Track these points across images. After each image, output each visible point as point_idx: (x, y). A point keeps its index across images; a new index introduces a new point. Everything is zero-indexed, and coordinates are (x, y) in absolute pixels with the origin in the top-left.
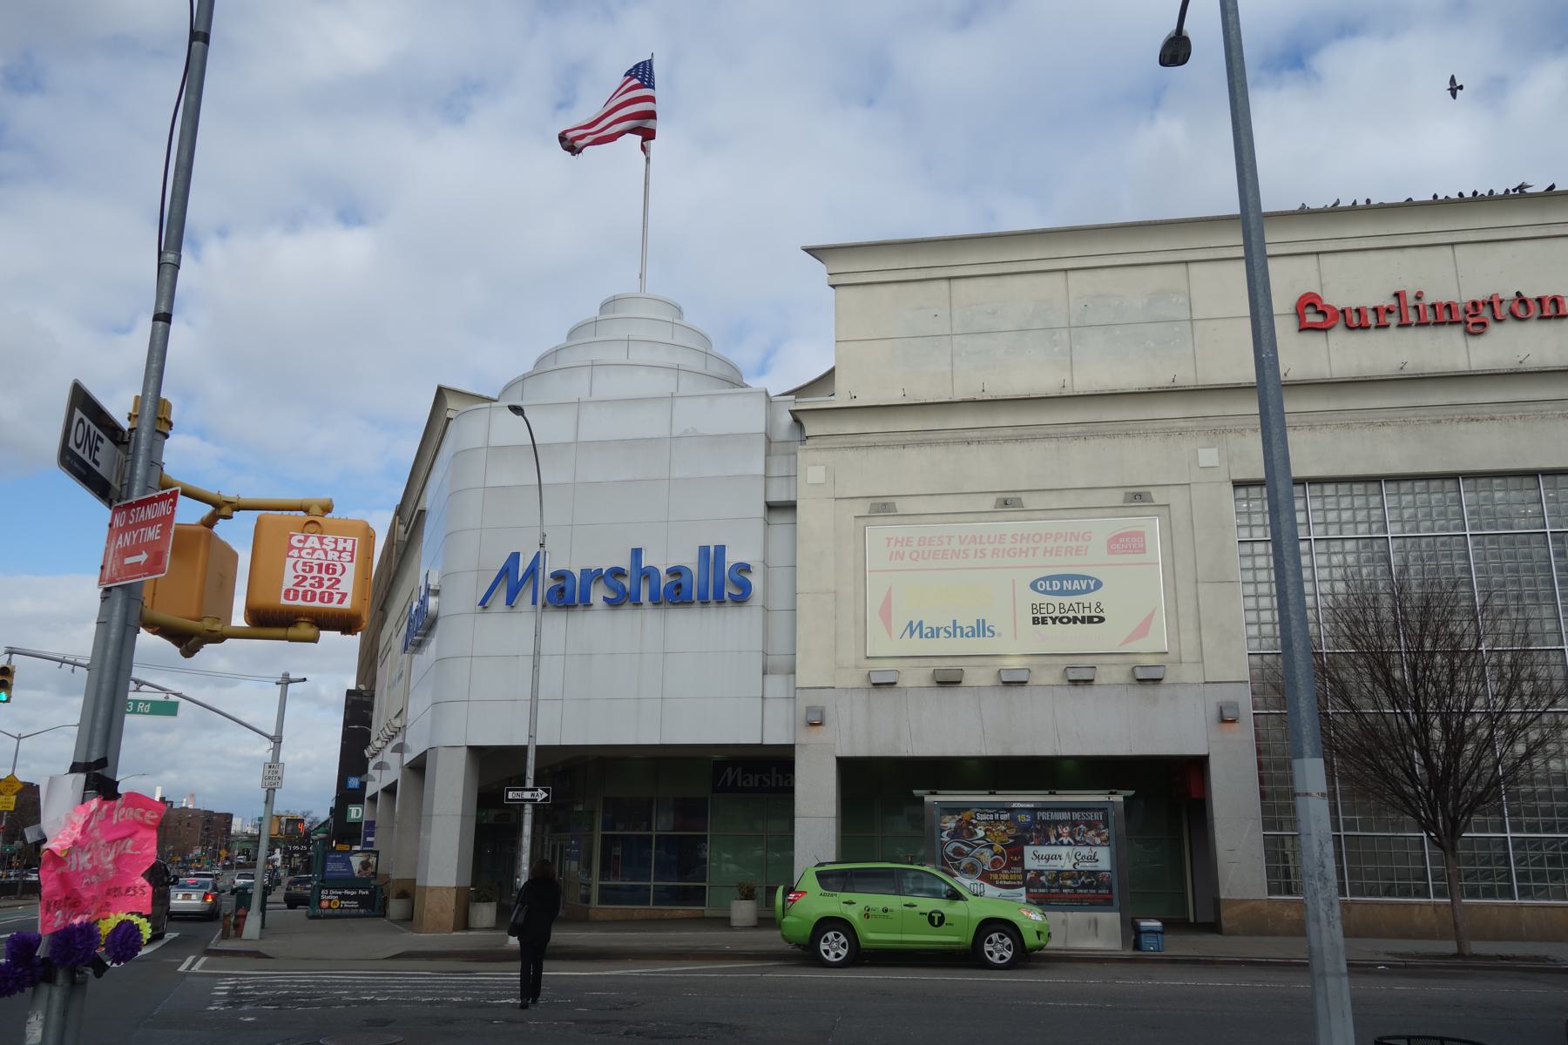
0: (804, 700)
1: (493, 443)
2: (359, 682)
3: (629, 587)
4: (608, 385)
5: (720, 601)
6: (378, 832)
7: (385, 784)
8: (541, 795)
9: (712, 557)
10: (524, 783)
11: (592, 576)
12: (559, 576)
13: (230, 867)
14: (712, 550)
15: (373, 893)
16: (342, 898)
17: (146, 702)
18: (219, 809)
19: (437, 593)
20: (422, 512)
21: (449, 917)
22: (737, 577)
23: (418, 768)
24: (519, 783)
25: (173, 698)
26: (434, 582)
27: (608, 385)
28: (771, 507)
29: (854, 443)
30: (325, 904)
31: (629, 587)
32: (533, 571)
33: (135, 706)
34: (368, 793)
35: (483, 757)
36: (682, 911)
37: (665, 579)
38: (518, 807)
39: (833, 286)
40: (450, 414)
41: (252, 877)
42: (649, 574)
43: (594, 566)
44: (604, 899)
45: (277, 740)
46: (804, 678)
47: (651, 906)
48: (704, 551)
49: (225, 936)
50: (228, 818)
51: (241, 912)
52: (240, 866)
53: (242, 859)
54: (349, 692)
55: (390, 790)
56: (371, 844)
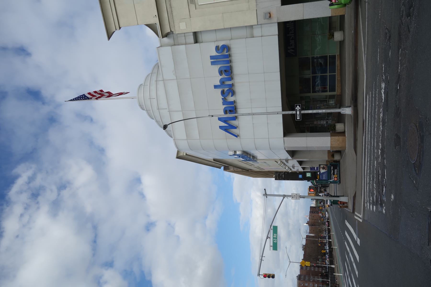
0: (262, 21)
1: (186, 138)
2: (272, 177)
3: (227, 89)
4: (163, 104)
5: (229, 56)
6: (313, 166)
7: (299, 165)
8: (298, 108)
9: (214, 60)
10: (294, 115)
11: (225, 101)
12: (226, 112)
13: (324, 206)
14: (212, 60)
15: (332, 165)
16: (334, 174)
17: (273, 235)
19: (235, 152)
20: (214, 160)
21: (340, 138)
22: (220, 51)
23: (293, 153)
24: (294, 116)
25: (272, 228)
26: (232, 153)
27: (163, 104)
28: (196, 41)
29: (170, 13)
31: (227, 89)
32: (225, 120)
33: (275, 238)
34: (302, 170)
35: (287, 132)
36: (338, 63)
37: (224, 76)
38: (303, 115)
39: (120, 28)
40: (185, 154)
41: (327, 201)
42: (222, 82)
43: (221, 101)
44: (334, 91)
45: (284, 196)
46: (254, 22)
47: (336, 74)
48: (213, 63)
49: (347, 207)
50: (311, 207)
51: (339, 203)
52: (324, 204)
53: (322, 203)
54: (276, 179)
55: (301, 163)
56: (317, 168)
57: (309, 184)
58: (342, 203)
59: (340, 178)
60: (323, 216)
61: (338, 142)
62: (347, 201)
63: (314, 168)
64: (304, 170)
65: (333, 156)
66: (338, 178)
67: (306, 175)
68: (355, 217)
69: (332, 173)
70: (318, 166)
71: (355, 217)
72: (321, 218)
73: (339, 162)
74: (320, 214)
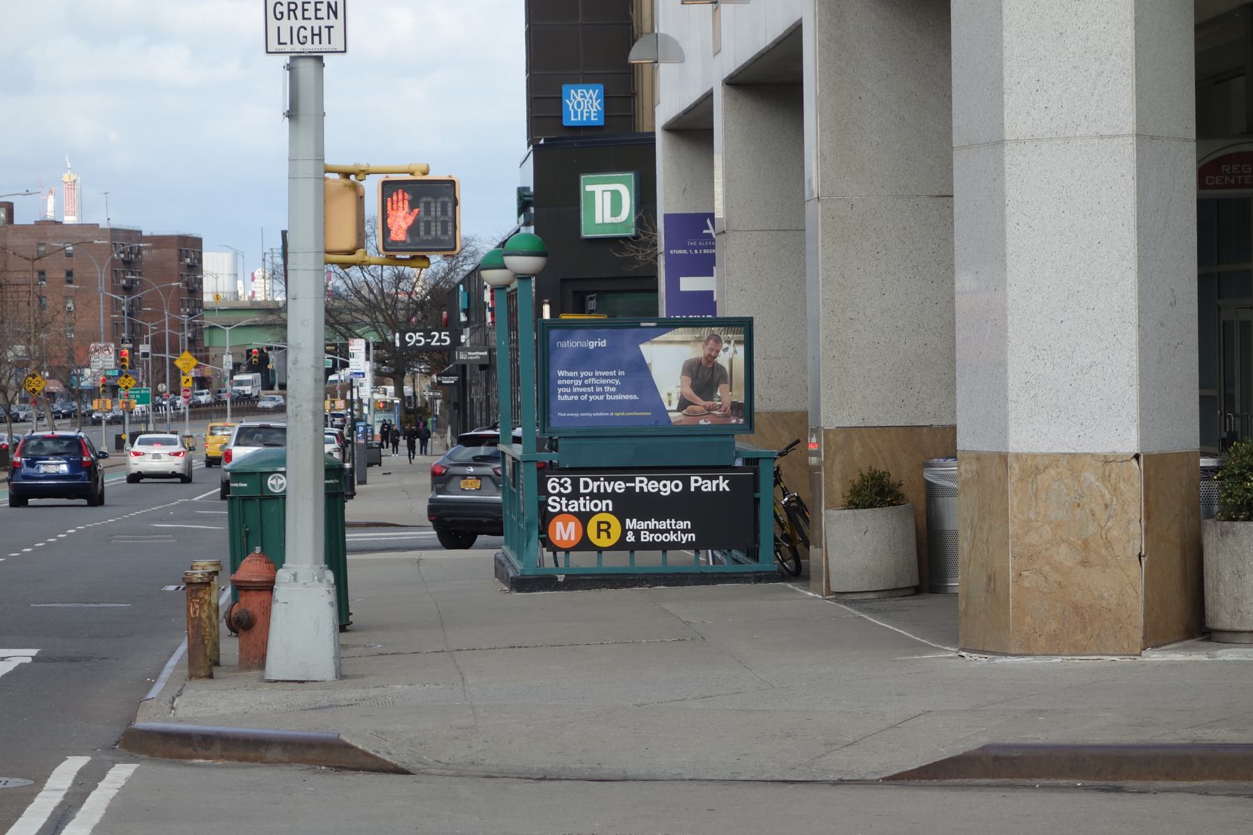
6: (728, 253)
13: (215, 410)
16: (628, 505)
18: (157, 222)
21: (1122, 578)
30: (564, 532)
49: (205, 664)
50: (188, 251)
51: (251, 569)
52: (245, 405)
53: (248, 383)
55: (771, 81)
56: (705, 300)
57: (490, 218)
58: (252, 602)
59: (577, 582)
60: (93, 393)
61: (1064, 556)
62: (277, 665)
63: (705, 266)
64: (671, 129)
65: (874, 492)
66: (583, 561)
67: (604, 165)
68: (72, 766)
69: (642, 484)
70: (727, 309)
71: (72, 766)
72: (66, 374)
73: (795, 566)
74: (103, 361)
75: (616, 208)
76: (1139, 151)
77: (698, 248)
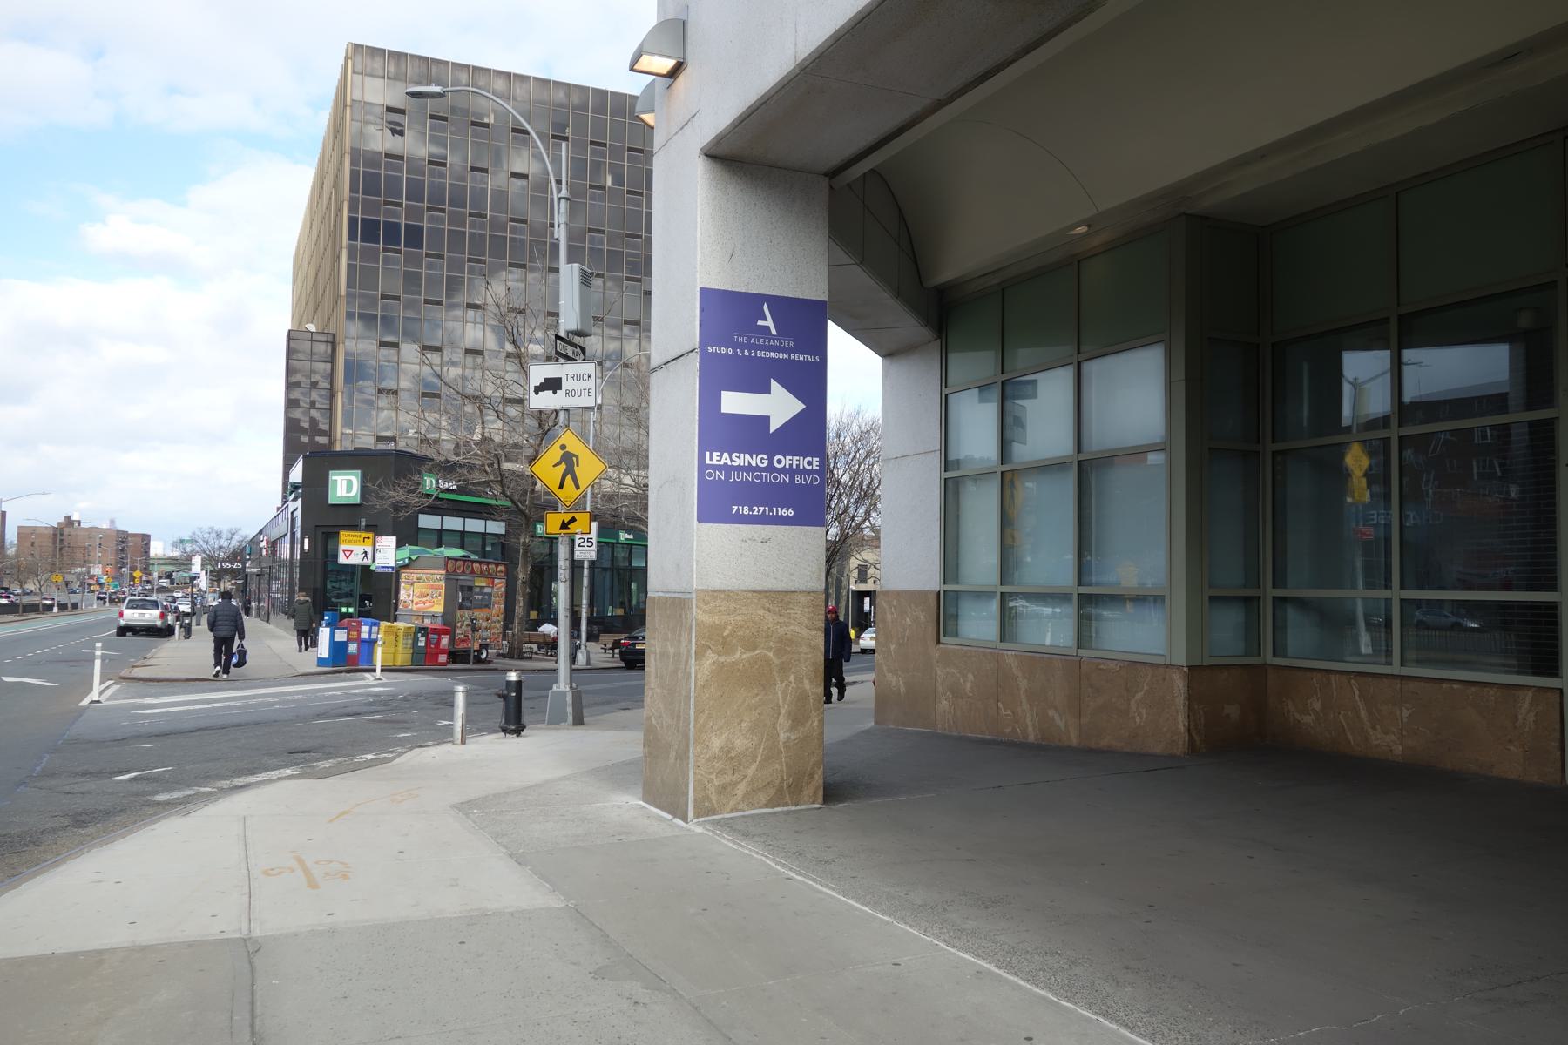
53: (165, 582)
75: (349, 489)
76: (200, 951)
77: (751, 347)
